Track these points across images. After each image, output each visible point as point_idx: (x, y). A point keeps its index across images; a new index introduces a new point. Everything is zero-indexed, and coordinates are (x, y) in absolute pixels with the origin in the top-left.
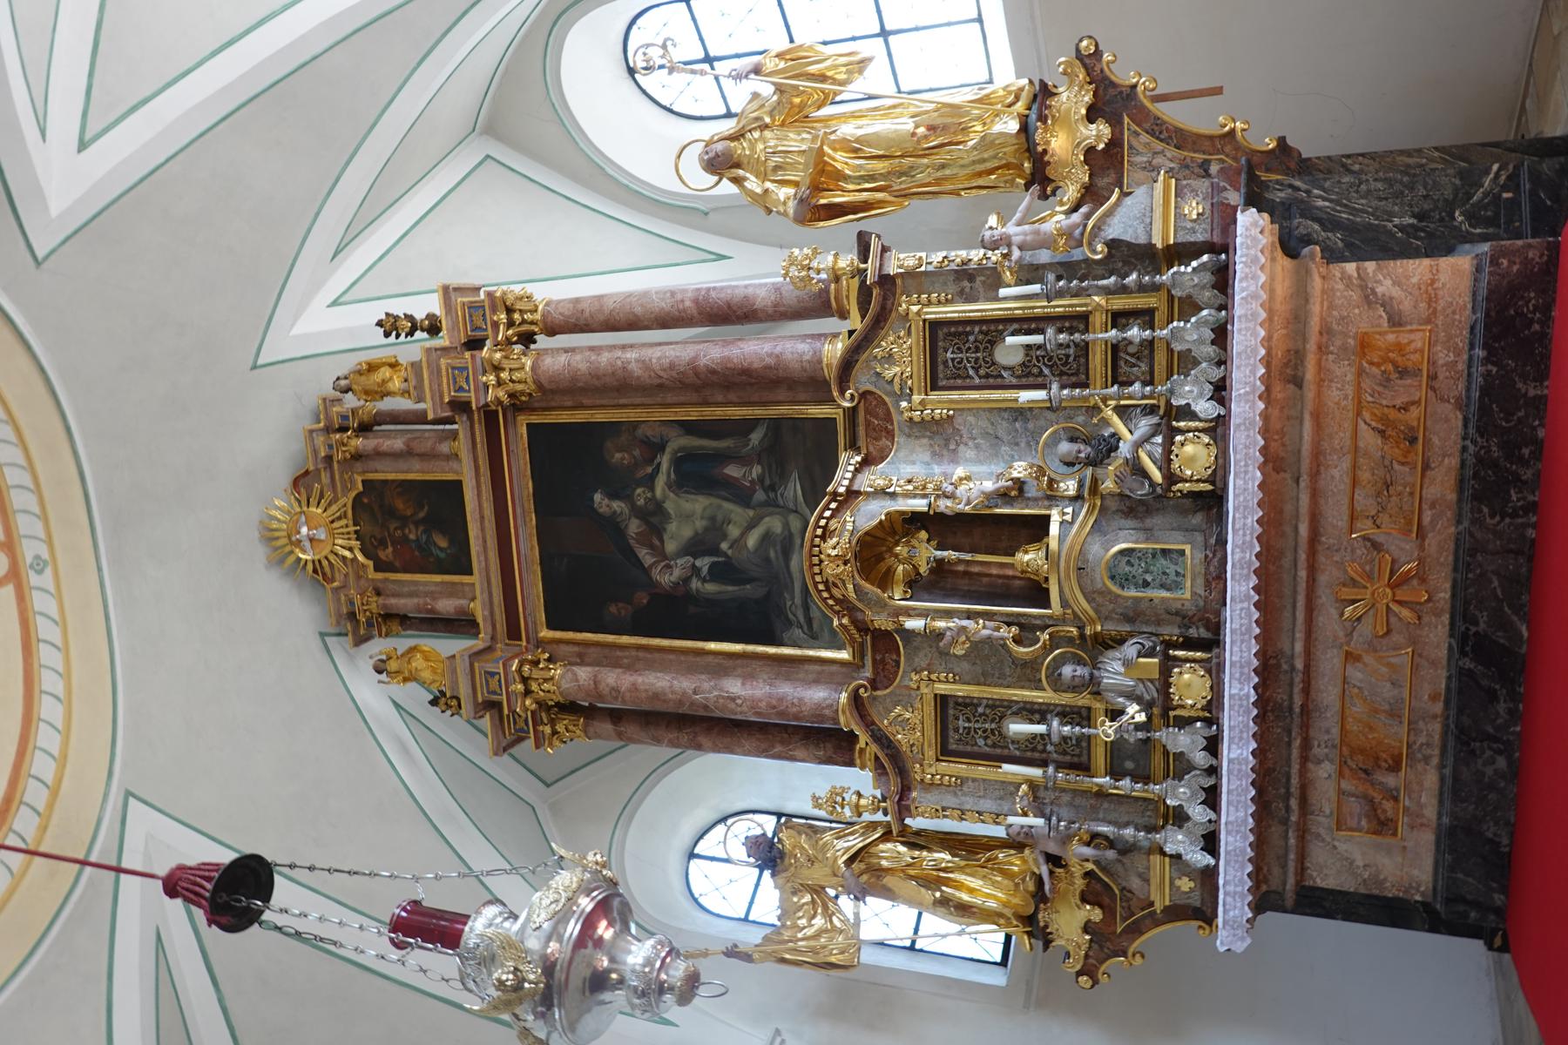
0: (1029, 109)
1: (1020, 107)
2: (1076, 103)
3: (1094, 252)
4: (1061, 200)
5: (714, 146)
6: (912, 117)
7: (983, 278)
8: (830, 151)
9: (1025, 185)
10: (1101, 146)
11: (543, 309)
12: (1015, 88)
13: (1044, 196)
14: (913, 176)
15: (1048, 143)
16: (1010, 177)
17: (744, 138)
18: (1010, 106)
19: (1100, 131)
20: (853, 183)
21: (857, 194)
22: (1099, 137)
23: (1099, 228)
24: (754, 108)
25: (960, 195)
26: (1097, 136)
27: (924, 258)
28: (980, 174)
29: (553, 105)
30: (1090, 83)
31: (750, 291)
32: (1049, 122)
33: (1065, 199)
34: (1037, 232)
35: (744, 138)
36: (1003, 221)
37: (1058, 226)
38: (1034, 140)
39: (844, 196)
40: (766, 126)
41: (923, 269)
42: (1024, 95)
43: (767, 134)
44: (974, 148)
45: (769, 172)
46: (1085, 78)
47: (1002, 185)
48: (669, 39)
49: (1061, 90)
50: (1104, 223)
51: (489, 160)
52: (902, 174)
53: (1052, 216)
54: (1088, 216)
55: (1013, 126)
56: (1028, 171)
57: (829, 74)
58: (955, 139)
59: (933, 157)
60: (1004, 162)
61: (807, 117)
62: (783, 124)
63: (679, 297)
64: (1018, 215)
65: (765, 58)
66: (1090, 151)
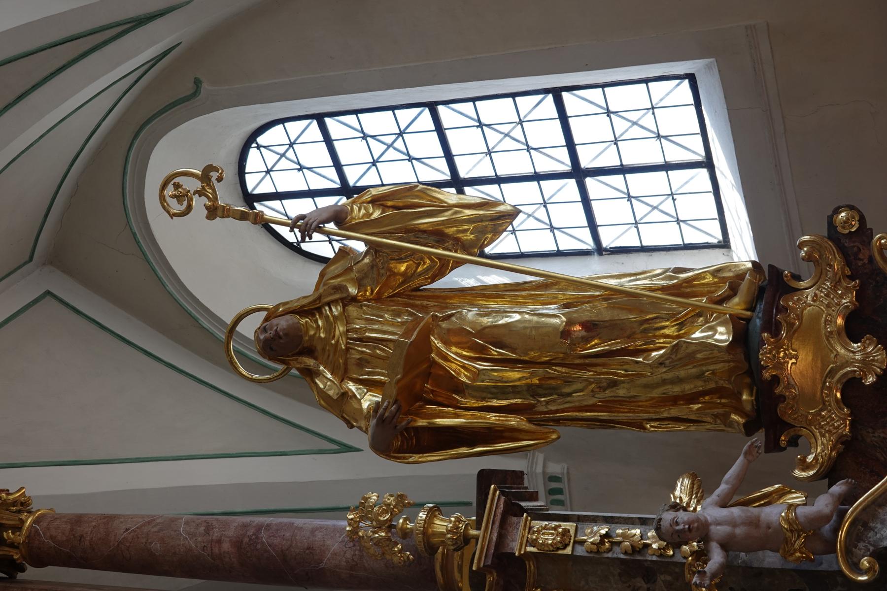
0: (752, 309)
1: (736, 305)
2: (828, 306)
3: (856, 567)
4: (804, 460)
5: (275, 321)
6: (566, 306)
7: (669, 578)
8: (440, 345)
9: (745, 425)
10: (871, 379)
11: (31, 526)
12: (731, 274)
13: (772, 445)
14: (569, 395)
15: (781, 366)
16: (721, 411)
17: (321, 313)
18: (721, 301)
19: (868, 355)
20: (473, 397)
21: (478, 414)
22: (866, 364)
23: (866, 525)
24: (337, 272)
25: (645, 428)
26: (863, 361)
27: (572, 533)
28: (674, 400)
29: (134, 235)
30: (852, 278)
31: (319, 535)
32: (784, 334)
33: (810, 458)
34: (754, 523)
35: (321, 313)
36: (701, 490)
37: (792, 515)
38: (758, 361)
39: (457, 416)
40: (354, 299)
41: (568, 551)
42: (744, 286)
43: (352, 310)
44: (660, 362)
45: (352, 367)
46: (843, 269)
47: (709, 419)
48: (216, 169)
49: (803, 284)
50: (874, 517)
51: (48, 297)
52: (552, 390)
53: (781, 494)
54: (847, 499)
55: (722, 335)
56: (748, 408)
57: (451, 231)
58: (631, 345)
59: (599, 369)
60: (712, 385)
61: (417, 289)
62: (378, 299)
63: (216, 534)
64: (723, 487)
65: (353, 202)
66: (851, 385)
